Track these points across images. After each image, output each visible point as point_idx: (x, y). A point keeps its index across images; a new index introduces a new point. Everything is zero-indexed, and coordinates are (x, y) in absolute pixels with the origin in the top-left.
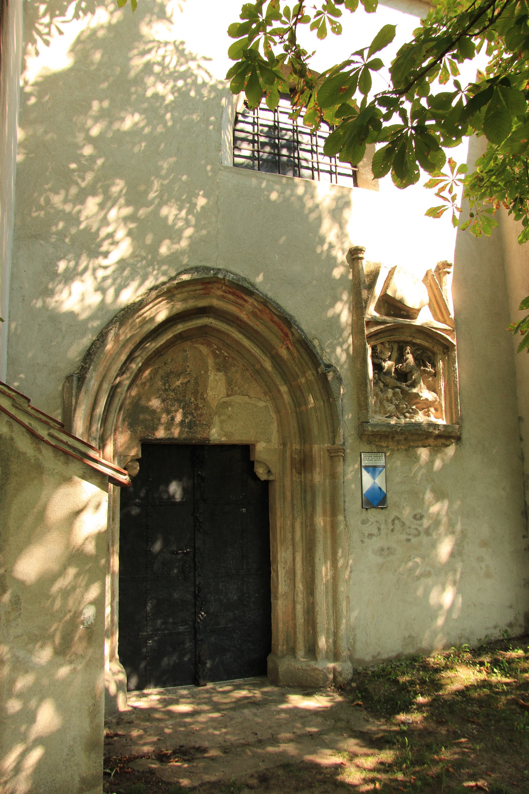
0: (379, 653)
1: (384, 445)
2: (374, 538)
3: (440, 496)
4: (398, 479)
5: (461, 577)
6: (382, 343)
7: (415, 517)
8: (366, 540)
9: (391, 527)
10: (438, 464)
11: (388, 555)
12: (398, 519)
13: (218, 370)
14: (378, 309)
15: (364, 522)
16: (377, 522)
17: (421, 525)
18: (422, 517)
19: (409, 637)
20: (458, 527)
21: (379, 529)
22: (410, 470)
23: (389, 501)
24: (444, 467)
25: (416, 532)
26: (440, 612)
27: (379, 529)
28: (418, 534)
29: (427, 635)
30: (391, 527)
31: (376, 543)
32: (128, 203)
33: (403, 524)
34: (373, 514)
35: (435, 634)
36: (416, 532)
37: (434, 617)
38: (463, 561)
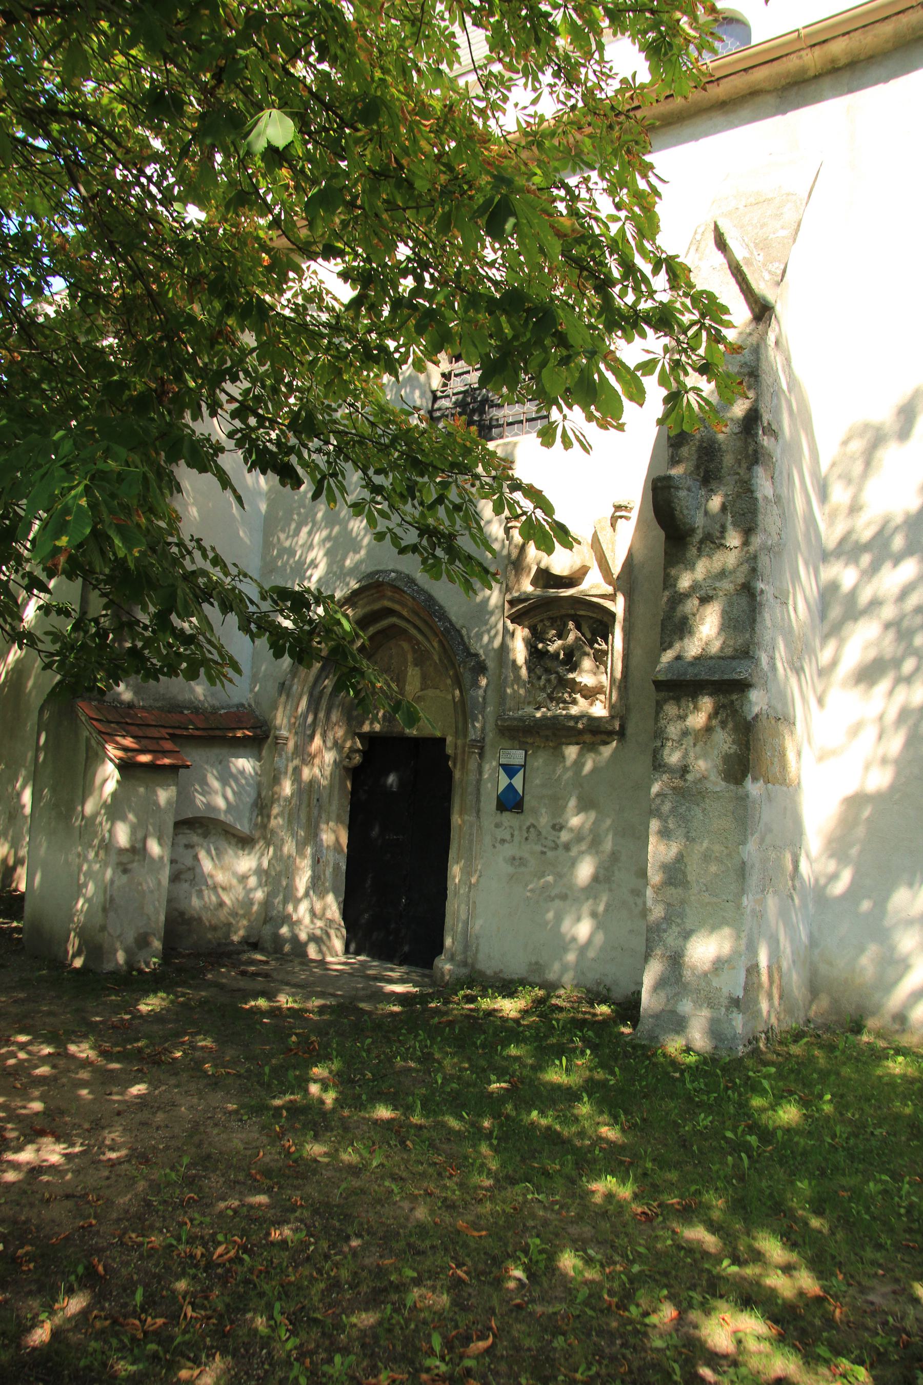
0: (501, 971)
1: (530, 740)
2: (506, 845)
3: (585, 805)
4: (538, 782)
5: (606, 910)
6: (542, 621)
7: (554, 827)
8: (498, 845)
9: (525, 835)
10: (588, 766)
11: (520, 865)
12: (534, 826)
13: (416, 665)
14: (534, 583)
15: (497, 826)
16: (511, 827)
17: (559, 837)
18: (561, 828)
19: (537, 963)
20: (608, 845)
21: (512, 836)
22: (554, 771)
23: (526, 806)
24: (594, 770)
25: (553, 845)
26: (573, 946)
27: (512, 836)
28: (556, 847)
29: (556, 966)
30: (525, 835)
31: (508, 850)
32: (326, 527)
33: (539, 834)
34: (508, 818)
35: (565, 968)
36: (553, 845)
37: (565, 949)
38: (610, 890)
